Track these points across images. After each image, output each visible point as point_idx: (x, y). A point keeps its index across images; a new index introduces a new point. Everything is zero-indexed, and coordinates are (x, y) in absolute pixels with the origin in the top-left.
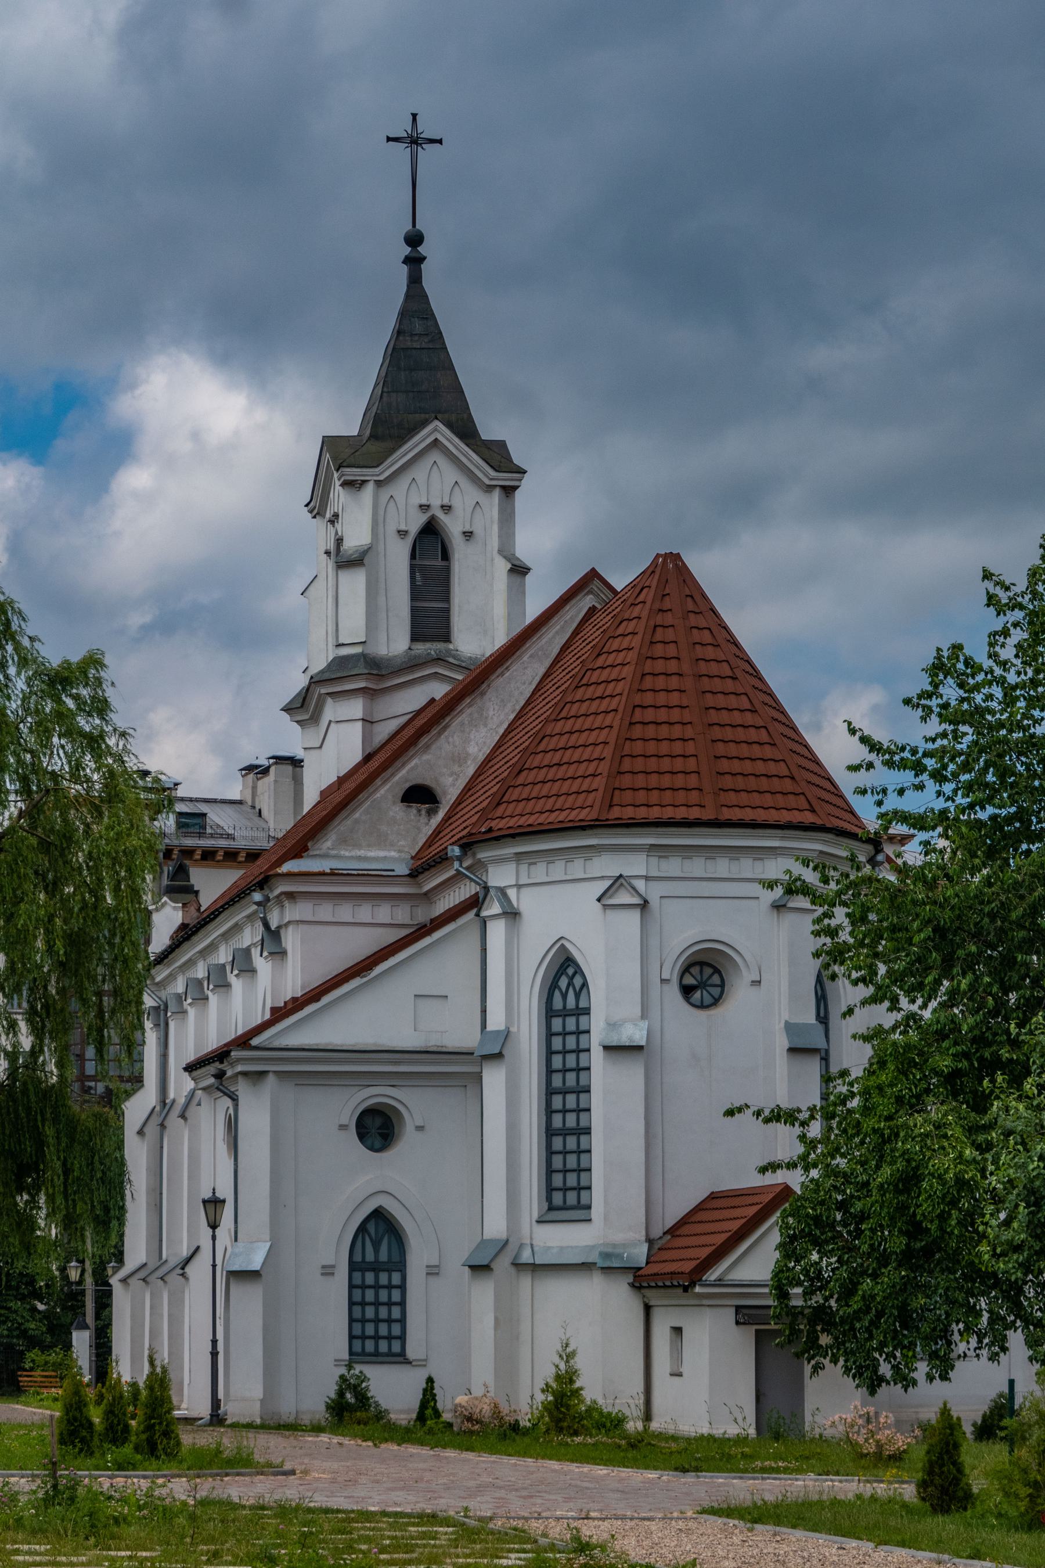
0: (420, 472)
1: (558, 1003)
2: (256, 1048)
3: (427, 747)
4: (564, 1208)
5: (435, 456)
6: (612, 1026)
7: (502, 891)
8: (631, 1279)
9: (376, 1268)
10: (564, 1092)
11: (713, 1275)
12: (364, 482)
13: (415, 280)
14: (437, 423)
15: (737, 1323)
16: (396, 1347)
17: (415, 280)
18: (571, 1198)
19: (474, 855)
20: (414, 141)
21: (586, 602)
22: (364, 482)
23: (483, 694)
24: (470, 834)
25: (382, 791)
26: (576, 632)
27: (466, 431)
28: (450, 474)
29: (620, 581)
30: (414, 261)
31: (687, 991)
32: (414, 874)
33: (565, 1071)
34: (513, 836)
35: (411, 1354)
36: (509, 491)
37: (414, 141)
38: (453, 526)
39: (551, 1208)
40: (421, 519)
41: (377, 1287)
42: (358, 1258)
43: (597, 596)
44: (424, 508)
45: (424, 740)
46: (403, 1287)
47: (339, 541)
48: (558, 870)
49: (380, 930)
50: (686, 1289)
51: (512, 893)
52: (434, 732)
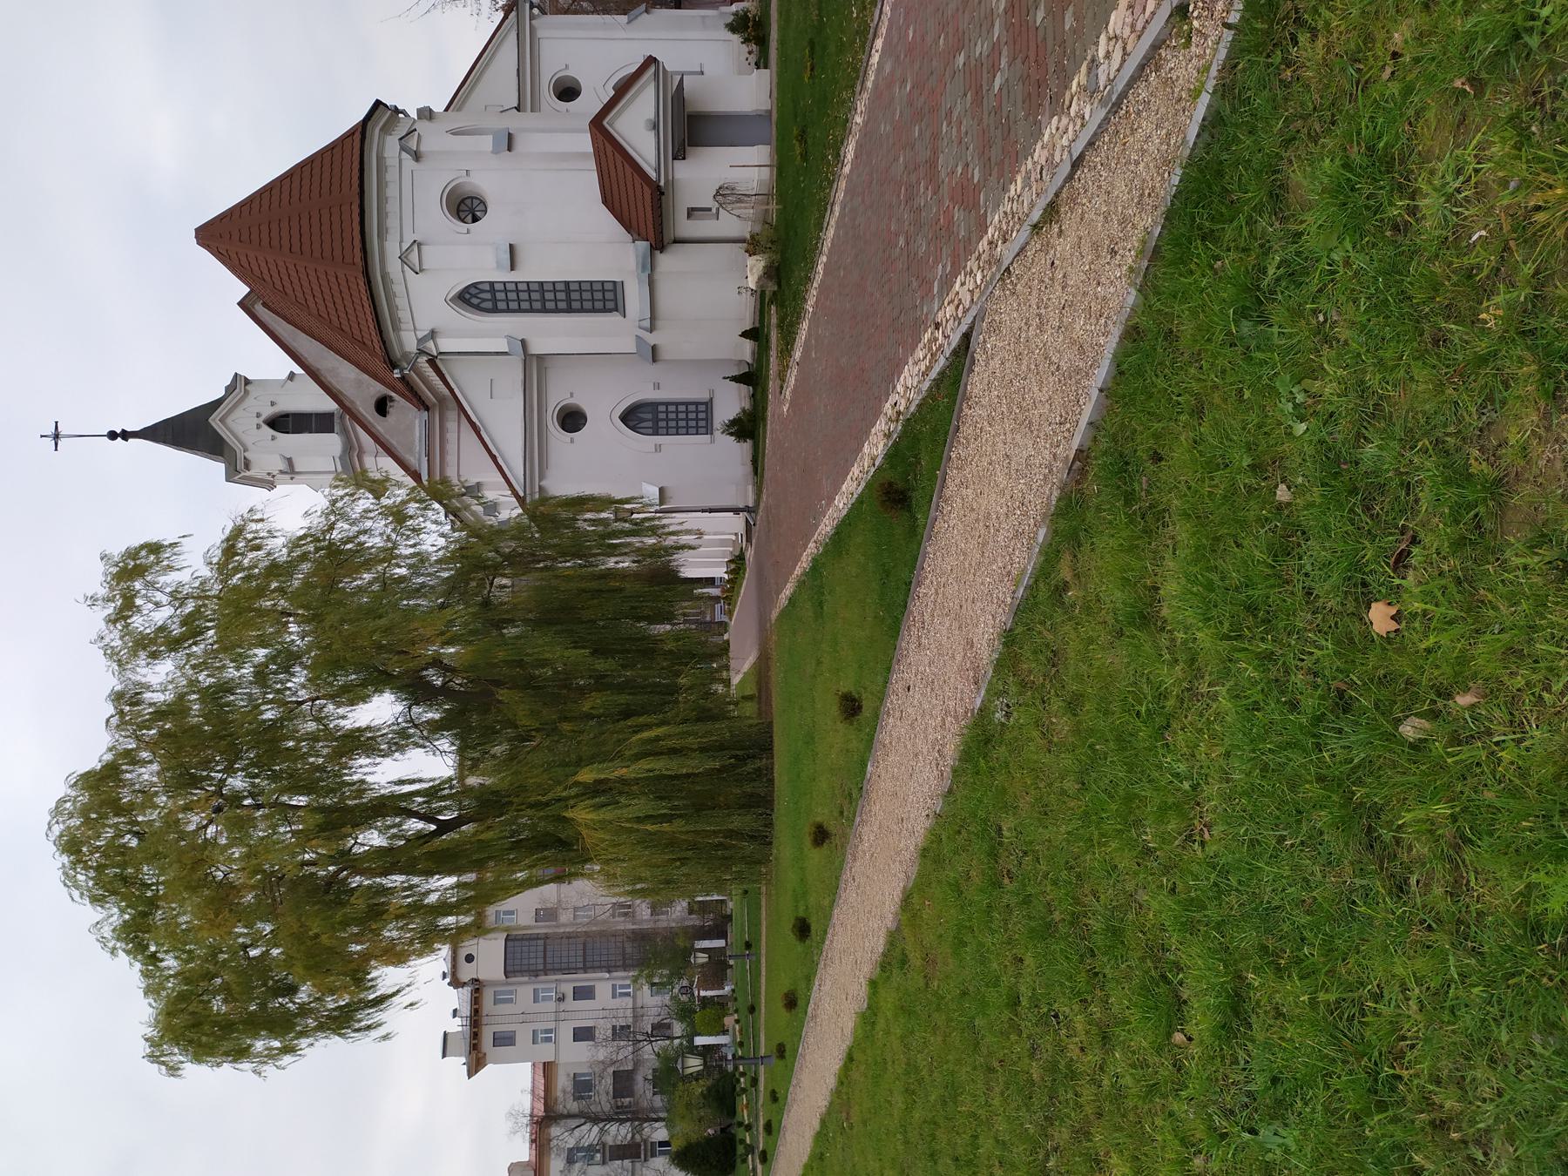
0: (238, 429)
1: (489, 305)
2: (525, 492)
3: (352, 402)
4: (615, 300)
5: (229, 421)
6: (499, 266)
7: (420, 341)
8: (658, 252)
9: (656, 420)
10: (544, 300)
11: (653, 175)
12: (245, 458)
13: (135, 435)
14: (210, 420)
15: (684, 159)
16: (702, 408)
17: (135, 435)
18: (609, 296)
19: (399, 360)
20: (56, 436)
21: (260, 309)
22: (245, 458)
23: (318, 369)
24: (385, 362)
25: (379, 428)
26: (277, 314)
27: (217, 404)
28: (238, 413)
29: (244, 290)
30: (125, 435)
31: (475, 219)
32: (427, 409)
33: (530, 300)
34: (381, 332)
35: (704, 396)
36: (247, 382)
37: (56, 436)
38: (268, 412)
39: (616, 310)
40: (266, 428)
41: (667, 420)
42: (651, 431)
43: (255, 302)
44: (258, 427)
45: (347, 404)
46: (667, 404)
47: (281, 472)
48: (401, 302)
49: (462, 429)
50: (663, 194)
51: (420, 335)
52: (342, 398)
